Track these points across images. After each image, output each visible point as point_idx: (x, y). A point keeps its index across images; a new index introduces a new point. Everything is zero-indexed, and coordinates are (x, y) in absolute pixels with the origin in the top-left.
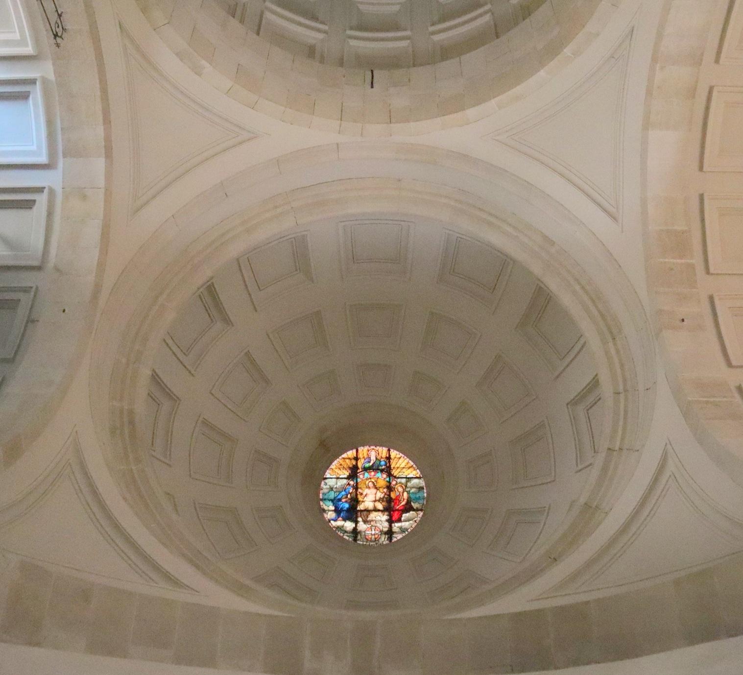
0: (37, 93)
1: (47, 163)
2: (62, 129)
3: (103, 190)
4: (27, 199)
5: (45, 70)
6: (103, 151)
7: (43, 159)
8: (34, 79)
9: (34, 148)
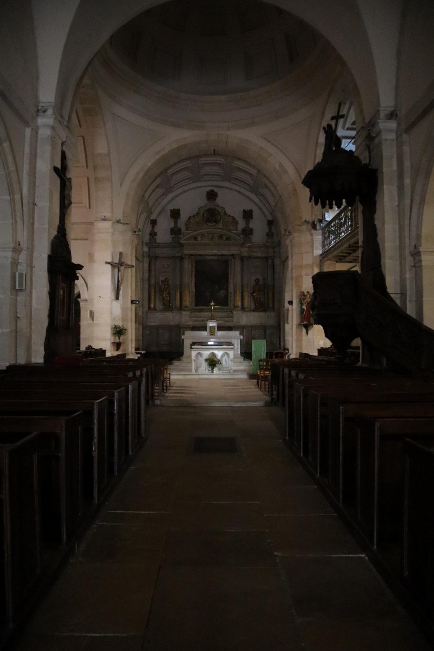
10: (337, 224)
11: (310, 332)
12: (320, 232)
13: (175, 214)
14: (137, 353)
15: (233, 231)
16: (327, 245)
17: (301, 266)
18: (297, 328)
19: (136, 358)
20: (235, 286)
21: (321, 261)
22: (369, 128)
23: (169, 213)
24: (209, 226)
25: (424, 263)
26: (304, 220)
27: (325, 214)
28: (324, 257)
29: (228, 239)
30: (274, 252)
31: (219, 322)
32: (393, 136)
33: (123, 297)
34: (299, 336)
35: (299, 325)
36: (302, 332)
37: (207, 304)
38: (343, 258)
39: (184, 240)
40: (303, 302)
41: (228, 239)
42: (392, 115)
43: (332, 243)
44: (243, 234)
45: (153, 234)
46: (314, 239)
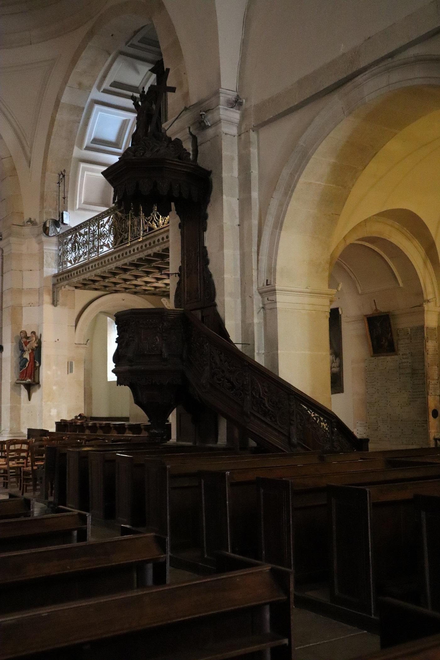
0: (87, 141)
1: (95, 105)
2: (79, 123)
3: (68, 85)
4: (115, 88)
5: (77, 152)
6: (60, 106)
7: (97, 107)
8: (86, 150)
9: (99, 113)
10: (93, 234)
11: (34, 395)
12: (55, 239)
16: (70, 262)
17: (20, 291)
18: (12, 389)
21: (54, 285)
22: (201, 113)
25: (279, 305)
26: (26, 218)
27: (62, 214)
28: (62, 280)
32: (234, 131)
34: (15, 400)
35: (16, 385)
36: (20, 394)
38: (91, 283)
40: (25, 348)
42: (236, 103)
43: (80, 261)
46: (45, 251)
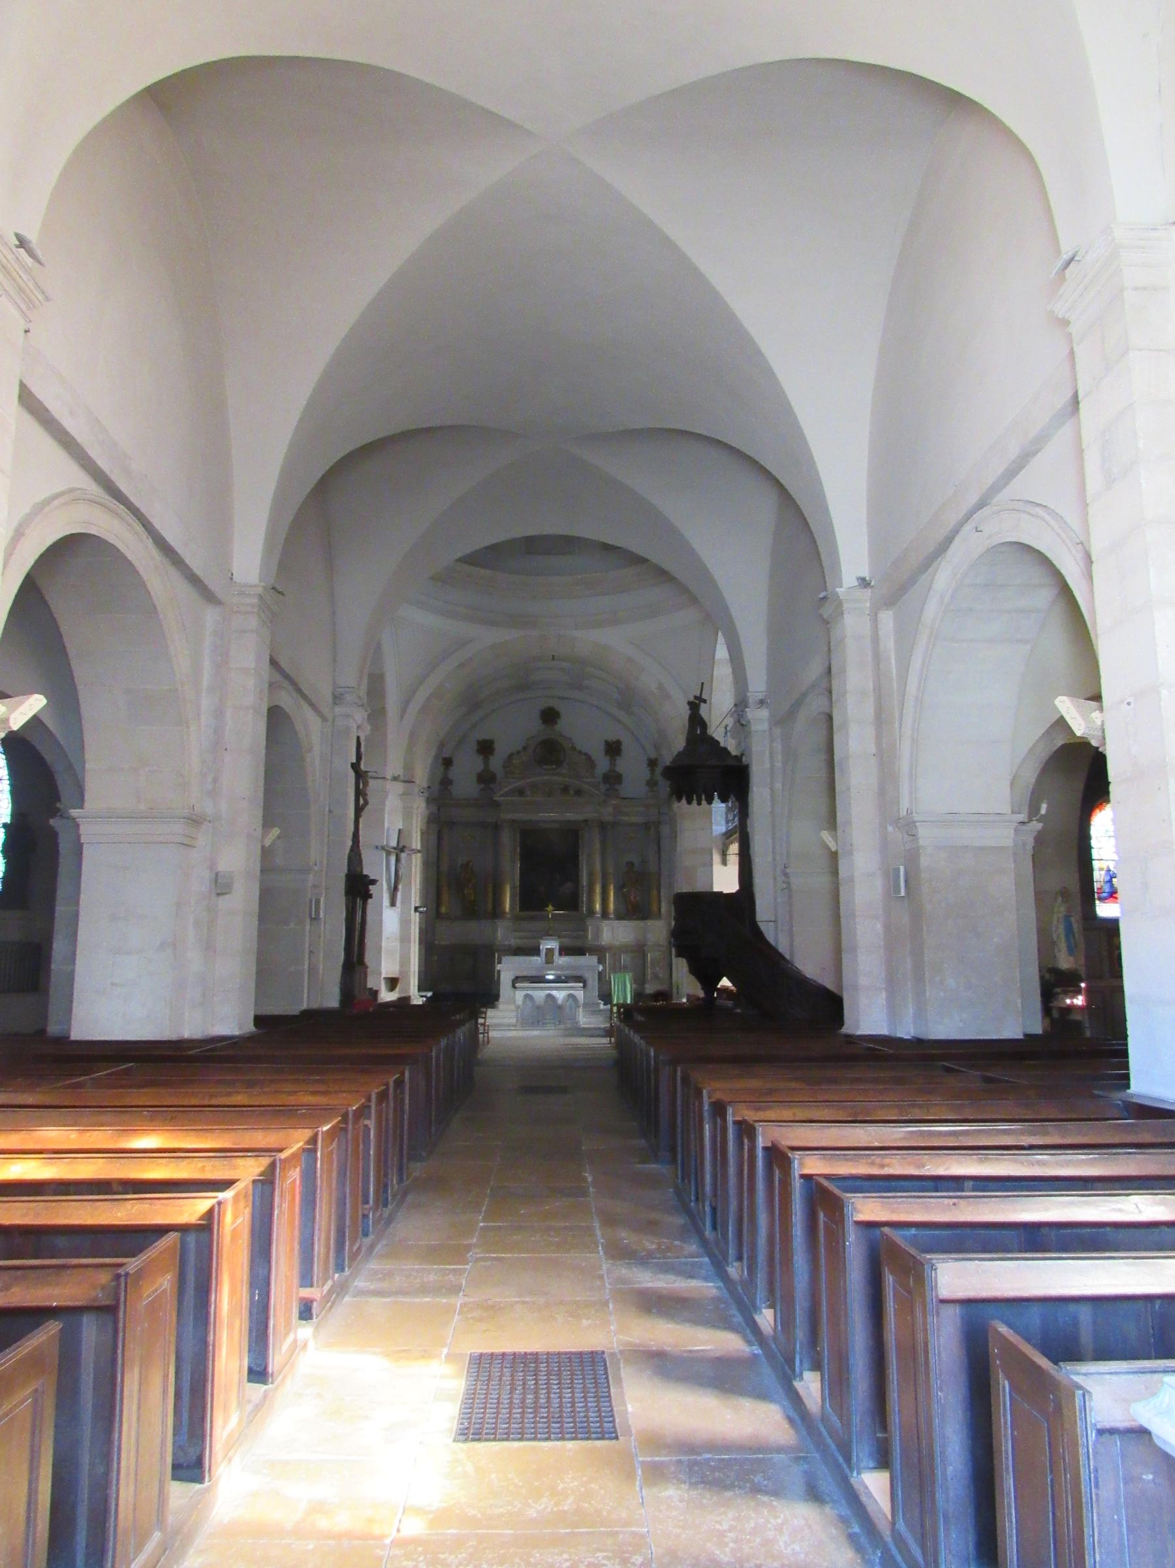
13: (486, 748)
14: (422, 996)
15: (585, 780)
19: (421, 1003)
20: (591, 875)
23: (475, 746)
24: (545, 769)
29: (579, 793)
30: (659, 813)
31: (564, 940)
32: (765, 726)
33: (402, 903)
37: (542, 907)
39: (502, 796)
41: (579, 793)
44: (605, 782)
45: (446, 782)
